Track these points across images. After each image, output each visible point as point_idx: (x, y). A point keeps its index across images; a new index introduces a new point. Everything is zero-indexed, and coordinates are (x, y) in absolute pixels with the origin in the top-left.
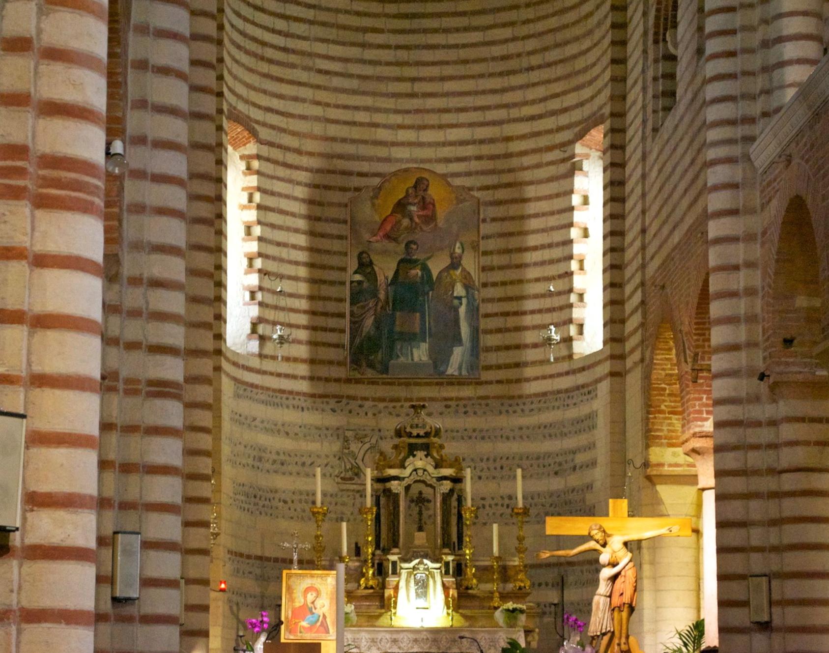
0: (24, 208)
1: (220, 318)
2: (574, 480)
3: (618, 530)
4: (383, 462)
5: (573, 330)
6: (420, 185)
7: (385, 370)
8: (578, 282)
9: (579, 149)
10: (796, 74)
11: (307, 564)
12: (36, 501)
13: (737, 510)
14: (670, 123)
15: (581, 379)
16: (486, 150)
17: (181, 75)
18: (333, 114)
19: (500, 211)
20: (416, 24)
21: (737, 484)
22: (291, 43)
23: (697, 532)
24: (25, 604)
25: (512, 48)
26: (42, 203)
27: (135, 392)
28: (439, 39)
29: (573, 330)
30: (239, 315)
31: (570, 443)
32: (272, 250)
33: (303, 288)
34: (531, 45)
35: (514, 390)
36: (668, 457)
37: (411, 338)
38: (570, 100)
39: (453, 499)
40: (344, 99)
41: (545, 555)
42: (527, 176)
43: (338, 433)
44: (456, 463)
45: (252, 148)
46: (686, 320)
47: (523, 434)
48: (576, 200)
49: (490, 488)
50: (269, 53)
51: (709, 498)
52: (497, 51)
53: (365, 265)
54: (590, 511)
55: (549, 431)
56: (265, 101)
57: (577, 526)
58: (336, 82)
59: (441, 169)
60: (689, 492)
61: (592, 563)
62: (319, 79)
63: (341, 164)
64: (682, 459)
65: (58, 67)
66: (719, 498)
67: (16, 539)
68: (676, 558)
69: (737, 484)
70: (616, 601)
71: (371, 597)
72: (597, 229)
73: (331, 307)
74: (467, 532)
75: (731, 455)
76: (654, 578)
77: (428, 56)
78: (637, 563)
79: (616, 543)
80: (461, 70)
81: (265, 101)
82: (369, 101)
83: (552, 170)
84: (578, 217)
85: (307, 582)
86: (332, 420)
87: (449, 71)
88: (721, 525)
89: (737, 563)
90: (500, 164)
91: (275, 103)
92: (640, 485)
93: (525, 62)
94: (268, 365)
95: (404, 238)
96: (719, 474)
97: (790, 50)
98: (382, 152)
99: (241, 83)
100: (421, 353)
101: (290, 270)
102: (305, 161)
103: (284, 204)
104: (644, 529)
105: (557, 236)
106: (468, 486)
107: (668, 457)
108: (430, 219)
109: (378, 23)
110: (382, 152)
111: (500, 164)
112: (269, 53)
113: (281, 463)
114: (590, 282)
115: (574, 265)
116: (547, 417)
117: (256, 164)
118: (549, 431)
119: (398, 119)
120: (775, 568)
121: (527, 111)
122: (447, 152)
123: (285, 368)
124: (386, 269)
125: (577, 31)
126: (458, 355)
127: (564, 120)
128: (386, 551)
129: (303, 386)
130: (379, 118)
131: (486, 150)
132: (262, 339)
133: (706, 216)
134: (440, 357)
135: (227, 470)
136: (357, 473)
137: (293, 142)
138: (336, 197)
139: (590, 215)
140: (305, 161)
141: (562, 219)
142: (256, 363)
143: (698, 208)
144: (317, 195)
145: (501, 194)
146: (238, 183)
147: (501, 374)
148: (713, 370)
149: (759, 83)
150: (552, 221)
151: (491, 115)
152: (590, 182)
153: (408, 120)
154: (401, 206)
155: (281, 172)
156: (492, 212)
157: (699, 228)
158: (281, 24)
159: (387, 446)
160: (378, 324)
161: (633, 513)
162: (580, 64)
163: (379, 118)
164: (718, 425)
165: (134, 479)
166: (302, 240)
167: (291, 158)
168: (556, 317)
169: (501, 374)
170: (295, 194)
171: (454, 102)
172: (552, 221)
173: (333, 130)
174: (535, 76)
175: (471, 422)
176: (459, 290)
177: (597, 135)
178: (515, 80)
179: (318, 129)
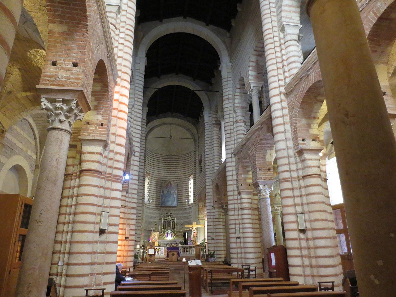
0: (110, 182)
1: (144, 198)
2: (189, 220)
3: (195, 226)
4: (165, 217)
5: (189, 200)
8: (190, 194)
9: (190, 177)
10: (217, 168)
11: (154, 231)
12: (110, 225)
13: (210, 224)
14: (201, 174)
15: (190, 206)
16: (178, 177)
17: (138, 166)
18: (159, 173)
19: (180, 185)
20: (170, 162)
21: (210, 220)
22: (154, 164)
23: (205, 226)
24: (107, 240)
25: (182, 165)
26: (113, 181)
27: (129, 208)
28: (173, 164)
29: (189, 200)
30: (146, 198)
31: (189, 215)
32: (151, 190)
33: (155, 195)
34: (184, 164)
35: (181, 208)
36: (201, 217)
38: (189, 171)
39: (174, 222)
40: (161, 171)
41: (185, 230)
42: (183, 181)
43: (159, 214)
44: (174, 217)
45: (149, 177)
46: (203, 199)
47: (183, 214)
48: (190, 184)
49: (178, 221)
50: (151, 165)
51: (206, 222)
52: (180, 165)
54: (191, 224)
55: (186, 213)
56: (150, 171)
57: (189, 226)
58: (160, 169)
59: (173, 180)
60: (204, 221)
61: (191, 231)
62: (158, 168)
63: (160, 179)
64: (203, 217)
65: (117, 162)
66: (207, 222)
67: (106, 231)
68: (202, 230)
69: (210, 220)
70: (194, 236)
71: (162, 236)
72: (192, 188)
73: (159, 197)
74: (175, 226)
75: (209, 217)
76: (199, 232)
77: (171, 166)
78: (197, 231)
79: (194, 228)
80: (176, 167)
81: (150, 171)
82: (164, 171)
83: (186, 180)
84: (190, 186)
85: (154, 234)
86: (158, 212)
87: (174, 168)
88: (208, 226)
89: (210, 231)
90: (180, 179)
91: (152, 171)
92: (198, 220)
93: (183, 167)
94: (150, 205)
96: (207, 219)
97: (216, 165)
98: (165, 177)
99: (148, 169)
101: (153, 192)
102: (155, 178)
103: (153, 184)
104: (198, 226)
105: (187, 188)
106: (175, 221)
107: (201, 217)
108: (171, 186)
109: (166, 162)
110: (165, 177)
111: (180, 179)
112: (151, 165)
113: (151, 218)
114: (191, 194)
115: (189, 192)
116: (186, 211)
117: (149, 179)
118: (186, 213)
119: (167, 173)
120: (215, 231)
121: (184, 173)
122: (173, 178)
123: (152, 205)
125: (190, 163)
127: (188, 174)
128: (165, 229)
129: (155, 207)
130: (165, 173)
131: (178, 177)
132: (149, 201)
133: (206, 186)
135: (144, 219)
136: (161, 219)
137: (154, 176)
138: (159, 183)
139: (191, 186)
140: (155, 178)
141: (188, 186)
142: (148, 204)
143: (205, 185)
144: (157, 183)
145: (180, 183)
146: (147, 181)
147: (180, 206)
148: (320, 139)
149: (213, 169)
150: (187, 186)
151: (179, 173)
152: (191, 182)
153: (169, 173)
155: (152, 180)
156: (179, 185)
157: (205, 188)
158: (153, 161)
159: (165, 215)
161: (197, 224)
162: (190, 167)
163: (165, 173)
164: (207, 213)
165: (307, 188)
166: (155, 188)
167: (154, 178)
168: (186, 199)
169: (180, 206)
170: (154, 183)
171: (175, 171)
172: (187, 186)
173: (159, 175)
174: (185, 168)
175: (176, 212)
177: (192, 176)
178: (183, 169)
179: (157, 174)
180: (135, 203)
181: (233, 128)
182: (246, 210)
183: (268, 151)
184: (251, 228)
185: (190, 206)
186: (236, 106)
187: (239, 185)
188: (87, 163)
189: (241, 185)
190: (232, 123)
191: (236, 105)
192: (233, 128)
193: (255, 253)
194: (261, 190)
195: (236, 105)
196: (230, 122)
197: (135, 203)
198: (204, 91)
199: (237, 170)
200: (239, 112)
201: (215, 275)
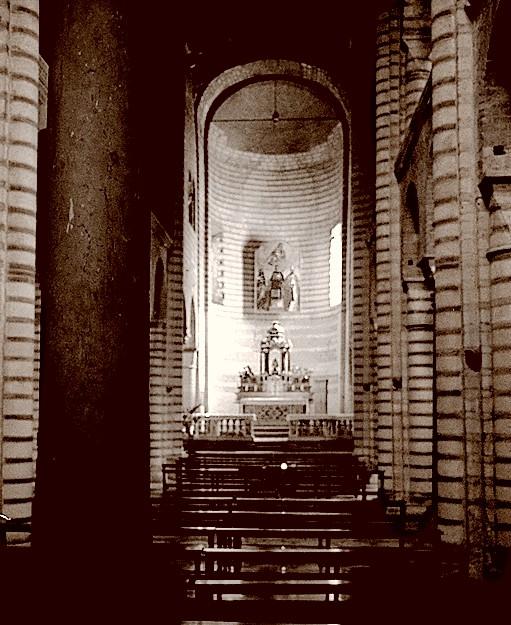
7: (268, 309)
35: (315, 316)
100: (280, 304)
108: (283, 257)
124: (268, 276)
160: (266, 292)
176: (293, 282)
181: (397, 121)
182: (421, 330)
186: (409, 29)
190: (396, 83)
192: (397, 121)
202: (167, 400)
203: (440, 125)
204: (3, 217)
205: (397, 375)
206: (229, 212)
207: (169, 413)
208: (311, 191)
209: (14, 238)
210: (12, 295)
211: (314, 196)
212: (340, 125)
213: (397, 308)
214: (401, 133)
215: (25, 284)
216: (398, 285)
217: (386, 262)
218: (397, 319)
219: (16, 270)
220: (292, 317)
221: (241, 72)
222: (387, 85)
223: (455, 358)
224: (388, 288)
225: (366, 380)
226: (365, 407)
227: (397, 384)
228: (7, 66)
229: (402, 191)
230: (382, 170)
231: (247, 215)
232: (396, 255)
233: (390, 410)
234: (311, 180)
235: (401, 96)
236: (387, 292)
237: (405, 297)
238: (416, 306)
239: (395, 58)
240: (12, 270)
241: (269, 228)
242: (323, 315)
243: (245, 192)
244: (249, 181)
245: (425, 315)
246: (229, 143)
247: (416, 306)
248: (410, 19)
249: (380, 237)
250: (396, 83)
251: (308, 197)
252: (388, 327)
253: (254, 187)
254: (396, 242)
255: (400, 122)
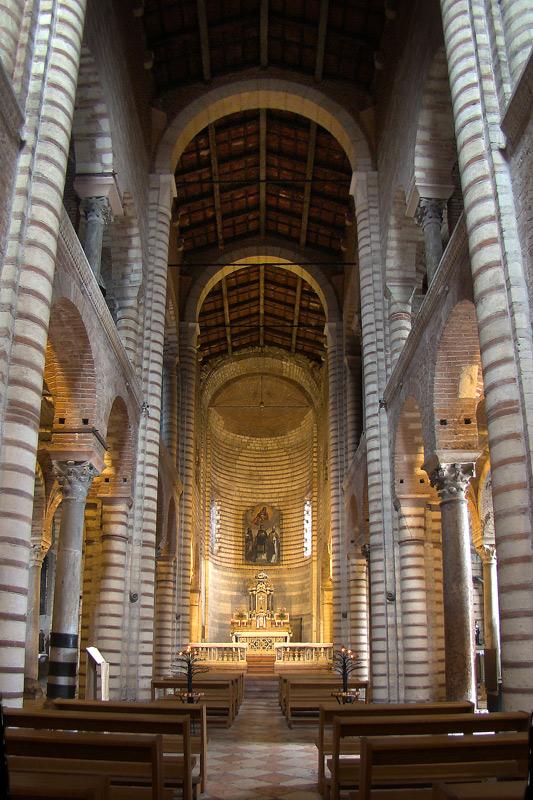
6: (264, 509)
15: (307, 562)
35: (292, 566)
37: (262, 552)
53: (250, 532)
95: (260, 524)
100: (264, 557)
108: (267, 518)
126: (274, 557)
134: (269, 557)
154: (259, 515)
176: (275, 539)
180: (118, 552)
181: (383, 357)
182: (412, 544)
183: (463, 368)
184: (423, 590)
185: (307, 562)
186: (391, 278)
187: (397, 481)
188: (116, 568)
189: (402, 482)
190: (380, 325)
191: (388, 273)
192: (383, 357)
193: (416, 516)
194: (445, 479)
195: (388, 273)
196: (376, 321)
197: (118, 552)
198: (317, 264)
199: (393, 443)
200: (396, 292)
201: (270, 683)
202: (176, 626)
203: (483, 264)
204: (3, 343)
205: (390, 588)
206: (225, 481)
207: (178, 638)
208: (287, 466)
209: (15, 371)
210: (9, 437)
211: (290, 471)
212: (310, 412)
213: (388, 526)
214: (387, 367)
215: (26, 427)
216: (389, 504)
217: (378, 484)
218: (389, 536)
219: (16, 408)
220: (273, 568)
221: (236, 367)
222: (373, 328)
223: (523, 517)
224: (379, 508)
225: (343, 609)
226: (343, 632)
227: (391, 598)
228: (20, 255)
229: (390, 418)
230: (371, 402)
231: (239, 485)
232: (387, 477)
233: (384, 623)
234: (287, 457)
235: (386, 336)
236: (380, 511)
237: (396, 514)
238: (408, 522)
239: (379, 305)
240: (12, 408)
241: (255, 496)
242: (297, 565)
243: (237, 466)
244: (240, 458)
245: (415, 530)
246: (226, 427)
247: (408, 522)
248: (391, 270)
249: (371, 462)
250: (380, 325)
251: (286, 471)
252: (380, 544)
253: (245, 463)
254: (386, 465)
255: (386, 357)
